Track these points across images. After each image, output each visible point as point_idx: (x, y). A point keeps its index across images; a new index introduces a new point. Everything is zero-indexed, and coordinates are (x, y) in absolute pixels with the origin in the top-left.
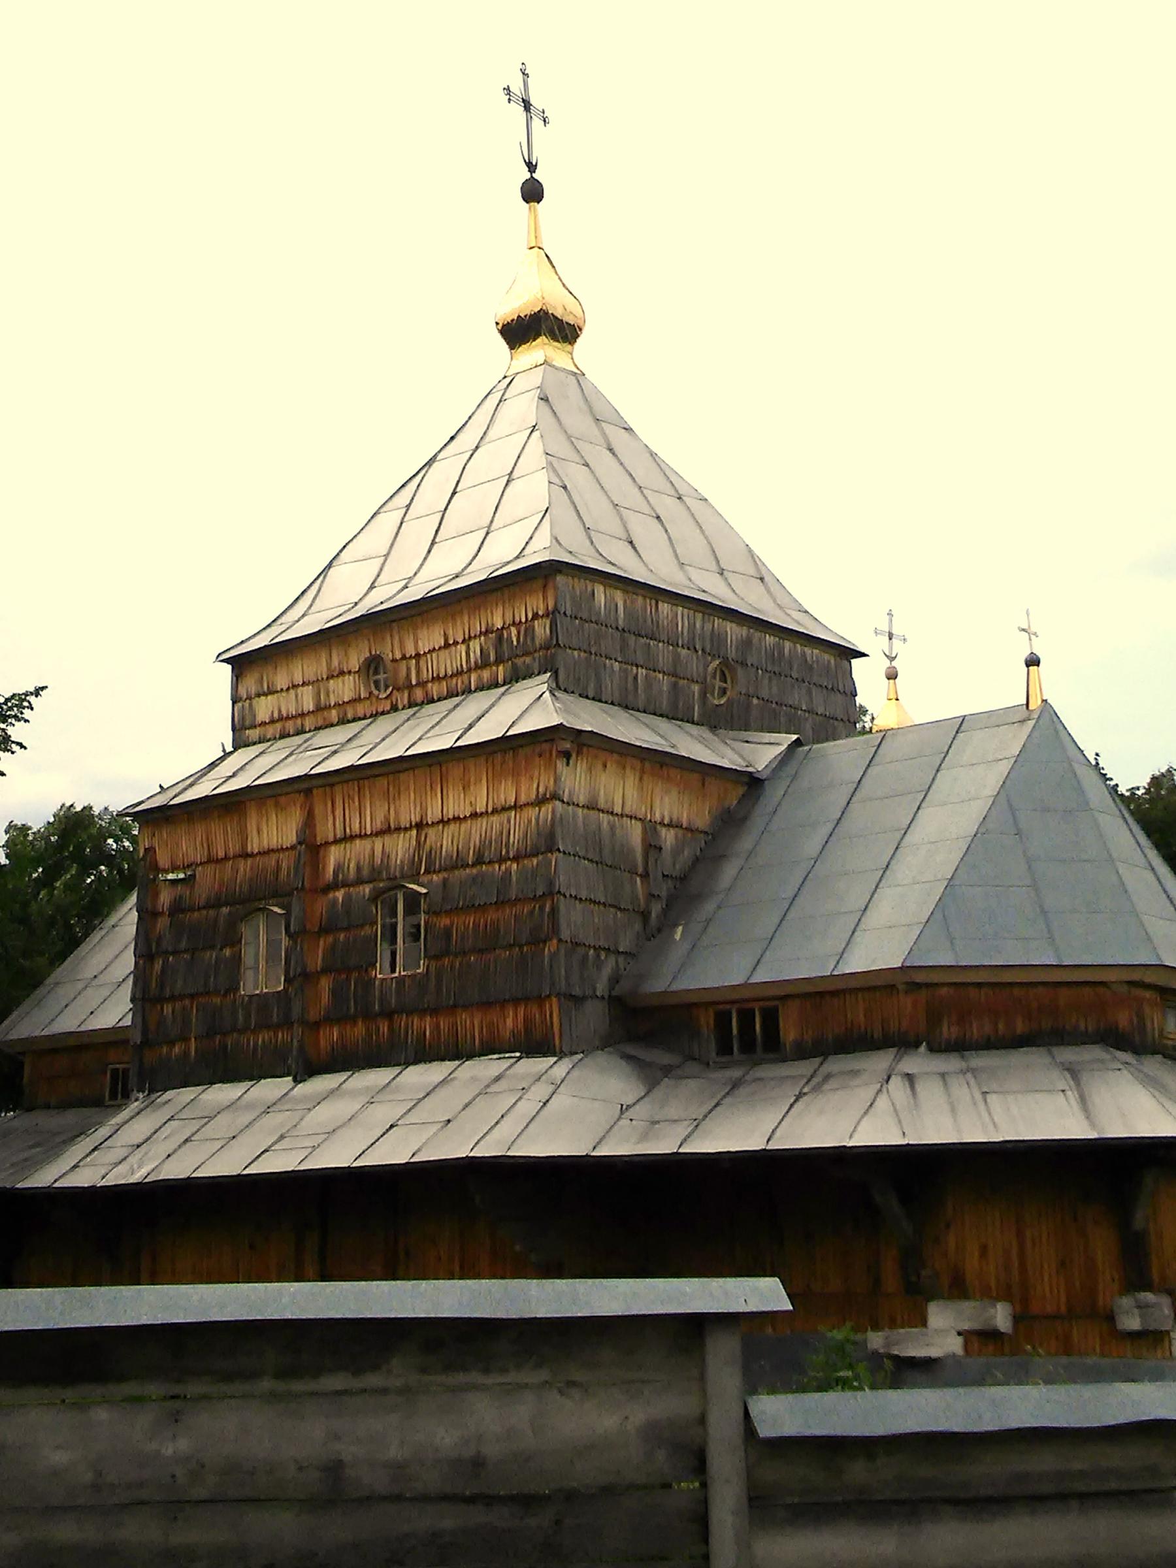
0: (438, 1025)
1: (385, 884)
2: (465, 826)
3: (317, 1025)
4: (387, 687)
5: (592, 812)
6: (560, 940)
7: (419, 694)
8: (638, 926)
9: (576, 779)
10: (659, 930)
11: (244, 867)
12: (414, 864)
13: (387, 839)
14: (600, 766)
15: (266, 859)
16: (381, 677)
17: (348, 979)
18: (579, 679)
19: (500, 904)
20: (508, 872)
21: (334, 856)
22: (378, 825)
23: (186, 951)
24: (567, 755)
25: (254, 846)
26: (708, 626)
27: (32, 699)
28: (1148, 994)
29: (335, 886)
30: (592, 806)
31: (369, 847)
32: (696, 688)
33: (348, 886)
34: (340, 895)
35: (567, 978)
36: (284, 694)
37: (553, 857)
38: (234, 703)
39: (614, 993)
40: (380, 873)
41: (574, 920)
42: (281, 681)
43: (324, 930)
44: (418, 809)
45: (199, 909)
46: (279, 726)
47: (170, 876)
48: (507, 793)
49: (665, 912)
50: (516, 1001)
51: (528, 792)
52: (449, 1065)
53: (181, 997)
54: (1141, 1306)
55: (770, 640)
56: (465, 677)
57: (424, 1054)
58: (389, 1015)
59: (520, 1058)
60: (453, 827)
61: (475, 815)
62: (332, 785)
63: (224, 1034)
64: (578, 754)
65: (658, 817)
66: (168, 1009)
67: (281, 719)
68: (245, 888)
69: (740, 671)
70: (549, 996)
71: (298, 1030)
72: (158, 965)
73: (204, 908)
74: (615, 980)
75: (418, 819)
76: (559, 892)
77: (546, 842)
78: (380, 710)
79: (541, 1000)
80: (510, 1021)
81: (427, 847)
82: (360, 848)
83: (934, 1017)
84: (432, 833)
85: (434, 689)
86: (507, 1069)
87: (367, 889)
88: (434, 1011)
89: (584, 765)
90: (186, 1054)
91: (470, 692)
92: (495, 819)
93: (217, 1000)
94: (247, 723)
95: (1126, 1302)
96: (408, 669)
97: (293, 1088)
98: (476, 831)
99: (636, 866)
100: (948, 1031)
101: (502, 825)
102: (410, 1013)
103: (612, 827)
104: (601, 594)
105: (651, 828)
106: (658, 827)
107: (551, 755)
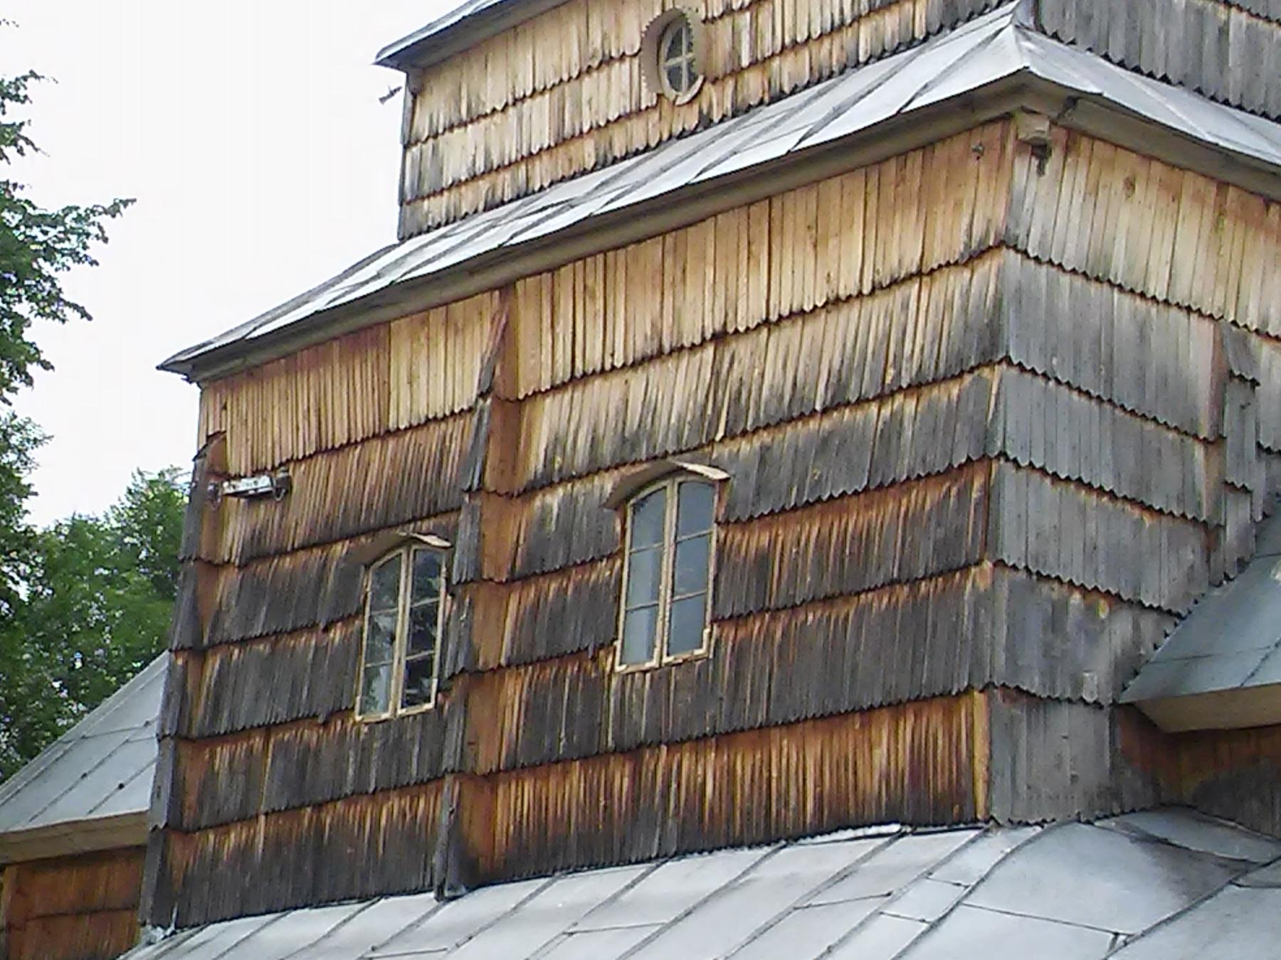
0: (731, 772)
1: (645, 470)
2: (813, 328)
3: (492, 778)
4: (692, 81)
5: (1094, 288)
6: (999, 564)
7: (753, 84)
8: (1191, 555)
9: (1060, 206)
10: (1242, 564)
11: (380, 457)
12: (706, 423)
13: (654, 370)
14: (1119, 185)
15: (421, 435)
16: (682, 60)
17: (558, 681)
18: (1090, 18)
19: (877, 490)
20: (897, 417)
21: (547, 420)
22: (642, 346)
23: (261, 637)
24: (1040, 150)
25: (400, 417)
27: (104, 220)
29: (545, 483)
31: (616, 395)
33: (572, 479)
34: (554, 500)
35: (1011, 649)
36: (497, 118)
37: (994, 376)
38: (406, 147)
39: (1125, 698)
40: (635, 446)
41: (1030, 518)
42: (493, 90)
43: (518, 579)
44: (720, 301)
45: (294, 550)
46: (483, 185)
47: (243, 485)
48: (904, 248)
49: (1259, 529)
50: (896, 707)
51: (950, 238)
52: (747, 856)
53: (246, 732)
56: (848, 35)
57: (701, 835)
58: (633, 751)
59: (901, 835)
60: (790, 333)
61: (835, 303)
62: (553, 270)
63: (319, 807)
64: (1067, 150)
66: (223, 755)
67: (489, 171)
68: (378, 502)
70: (968, 690)
71: (450, 787)
72: (214, 664)
73: (303, 548)
74: (1129, 667)
75: (718, 327)
76: (1003, 454)
77: (985, 348)
78: (677, 130)
79: (949, 699)
80: (883, 752)
81: (735, 375)
82: (603, 394)
84: (742, 348)
85: (788, 70)
86: (864, 859)
87: (607, 484)
88: (725, 738)
89: (1081, 179)
90: (244, 851)
91: (857, 65)
92: (877, 306)
93: (311, 736)
94: (426, 189)
96: (735, 33)
97: (435, 911)
98: (834, 338)
99: (1194, 422)
101: (889, 315)
102: (675, 744)
107: (1003, 148)
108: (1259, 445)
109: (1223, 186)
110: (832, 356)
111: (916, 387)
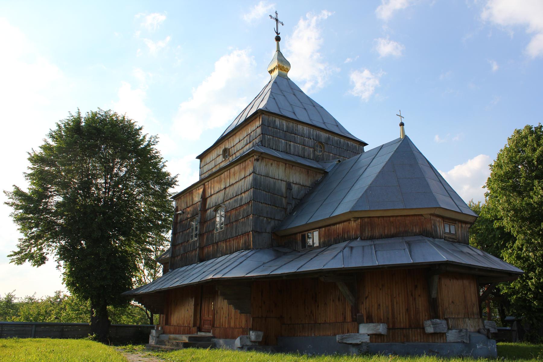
14: (270, 164)
26: (315, 133)
28: (438, 219)
30: (267, 176)
32: (311, 150)
54: (435, 325)
55: (336, 138)
65: (291, 181)
69: (326, 146)
83: (362, 227)
95: (429, 322)
100: (367, 233)
103: (275, 183)
104: (278, 121)
105: (289, 186)
106: (292, 184)
108: (293, 198)
109: (286, 164)
110: (236, 189)
111: (244, 192)
